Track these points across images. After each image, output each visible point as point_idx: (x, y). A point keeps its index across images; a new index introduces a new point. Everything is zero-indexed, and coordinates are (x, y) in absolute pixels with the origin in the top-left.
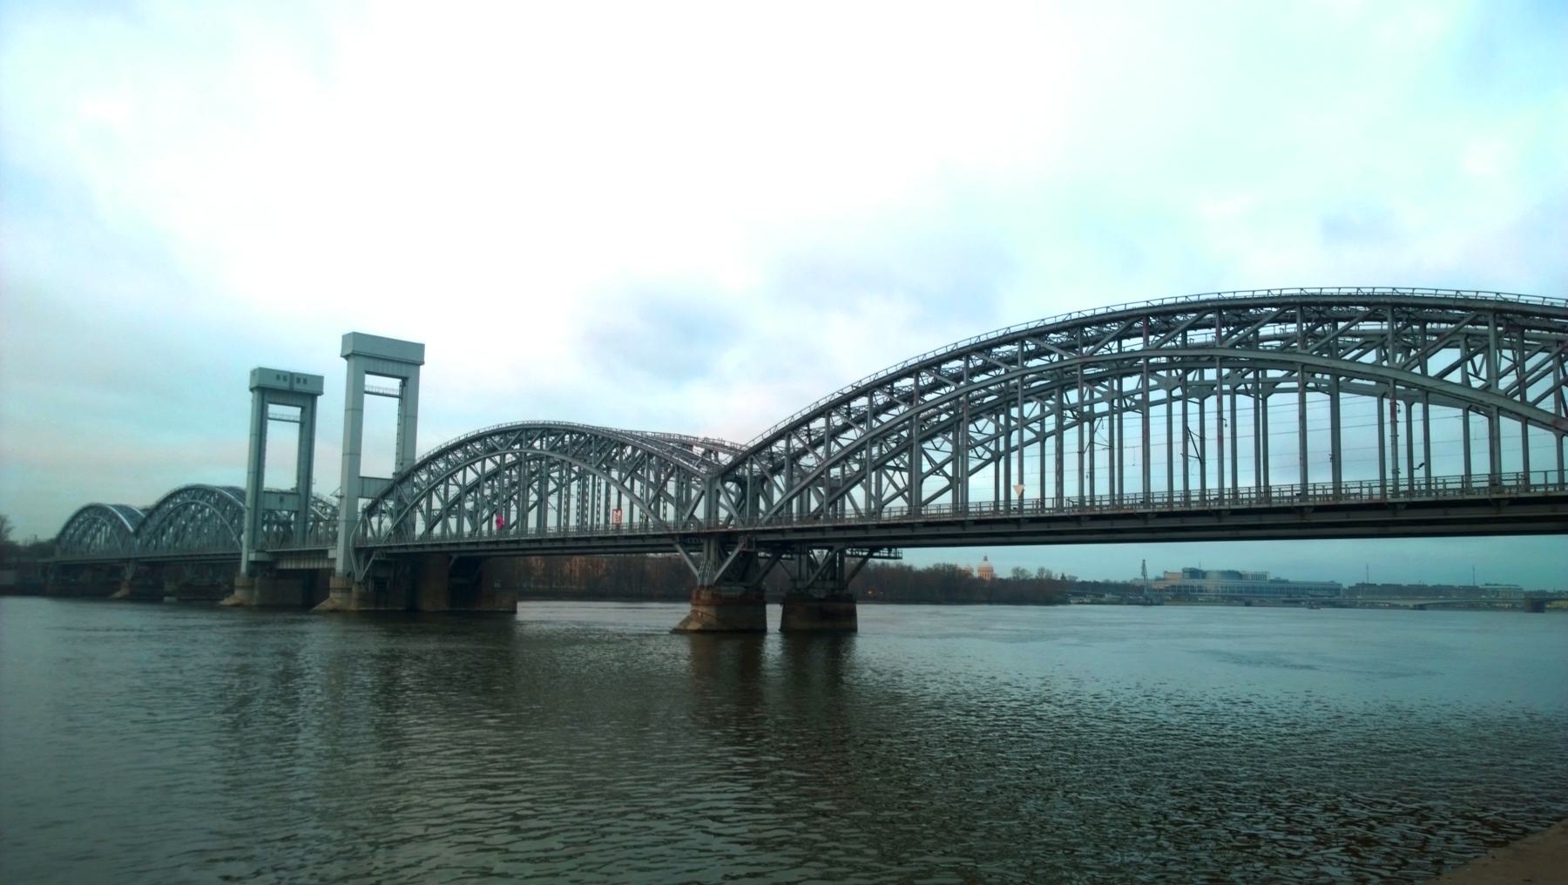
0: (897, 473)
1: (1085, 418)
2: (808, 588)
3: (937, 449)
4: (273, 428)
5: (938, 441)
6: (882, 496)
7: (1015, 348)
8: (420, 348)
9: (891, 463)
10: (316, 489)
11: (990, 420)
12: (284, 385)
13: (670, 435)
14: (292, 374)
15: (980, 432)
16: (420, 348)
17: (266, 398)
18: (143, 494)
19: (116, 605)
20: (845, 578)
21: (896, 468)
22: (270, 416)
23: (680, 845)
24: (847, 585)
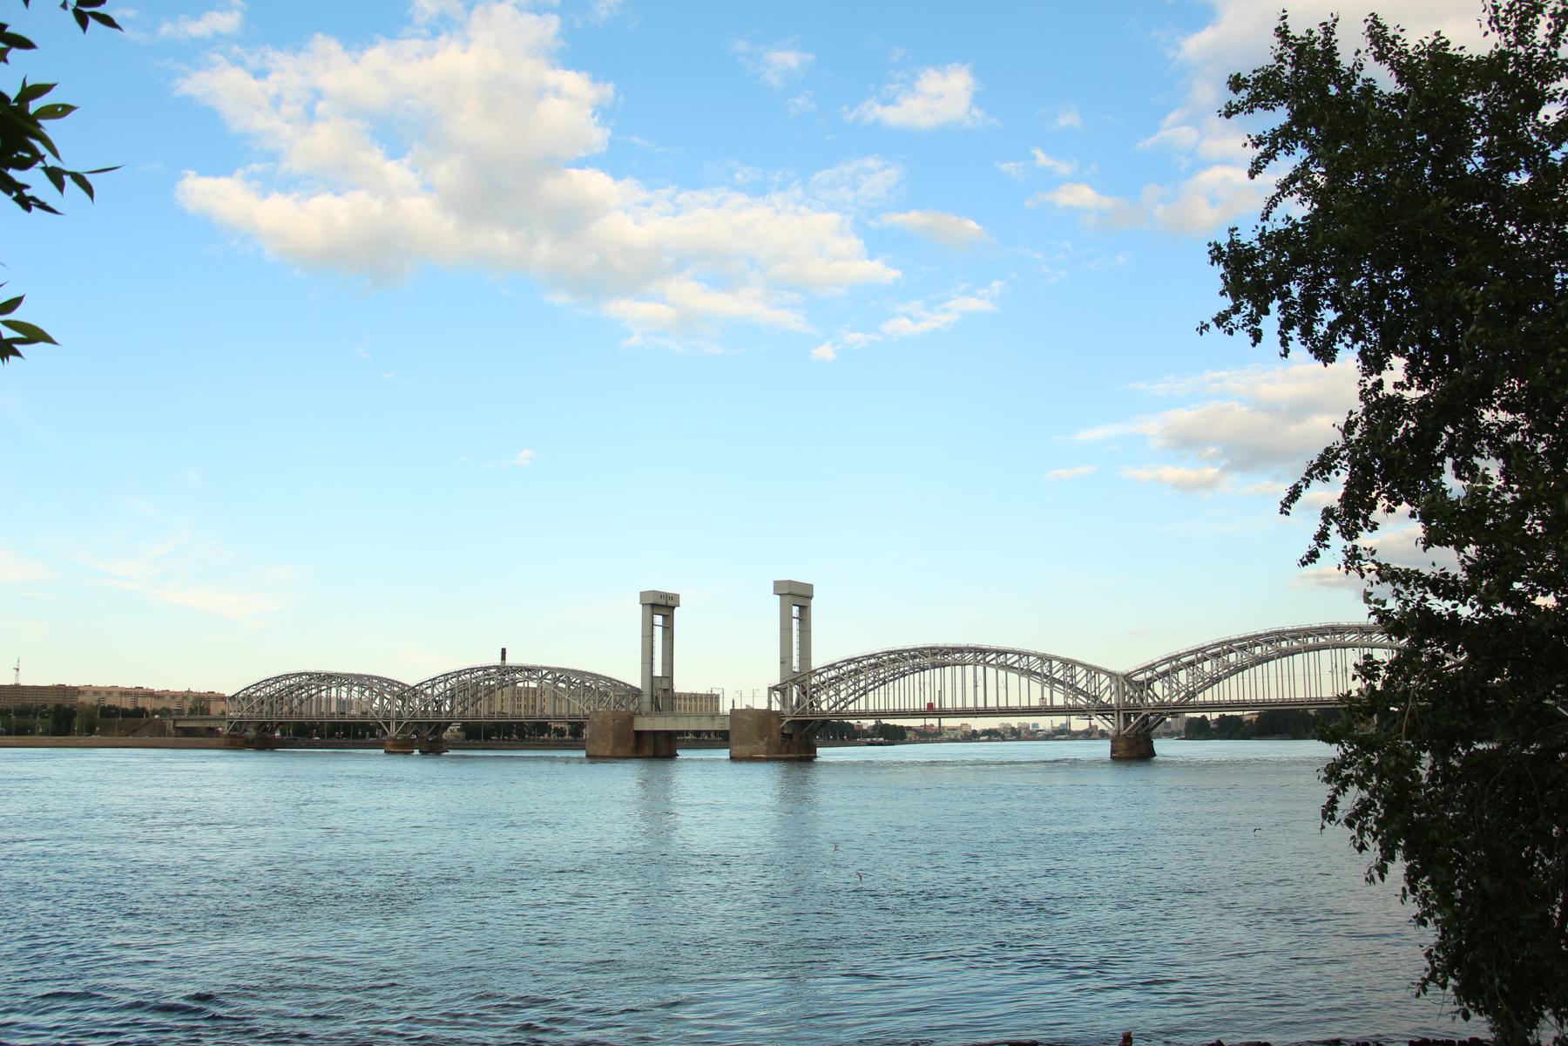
12: (663, 602)
14: (667, 594)
17: (655, 612)
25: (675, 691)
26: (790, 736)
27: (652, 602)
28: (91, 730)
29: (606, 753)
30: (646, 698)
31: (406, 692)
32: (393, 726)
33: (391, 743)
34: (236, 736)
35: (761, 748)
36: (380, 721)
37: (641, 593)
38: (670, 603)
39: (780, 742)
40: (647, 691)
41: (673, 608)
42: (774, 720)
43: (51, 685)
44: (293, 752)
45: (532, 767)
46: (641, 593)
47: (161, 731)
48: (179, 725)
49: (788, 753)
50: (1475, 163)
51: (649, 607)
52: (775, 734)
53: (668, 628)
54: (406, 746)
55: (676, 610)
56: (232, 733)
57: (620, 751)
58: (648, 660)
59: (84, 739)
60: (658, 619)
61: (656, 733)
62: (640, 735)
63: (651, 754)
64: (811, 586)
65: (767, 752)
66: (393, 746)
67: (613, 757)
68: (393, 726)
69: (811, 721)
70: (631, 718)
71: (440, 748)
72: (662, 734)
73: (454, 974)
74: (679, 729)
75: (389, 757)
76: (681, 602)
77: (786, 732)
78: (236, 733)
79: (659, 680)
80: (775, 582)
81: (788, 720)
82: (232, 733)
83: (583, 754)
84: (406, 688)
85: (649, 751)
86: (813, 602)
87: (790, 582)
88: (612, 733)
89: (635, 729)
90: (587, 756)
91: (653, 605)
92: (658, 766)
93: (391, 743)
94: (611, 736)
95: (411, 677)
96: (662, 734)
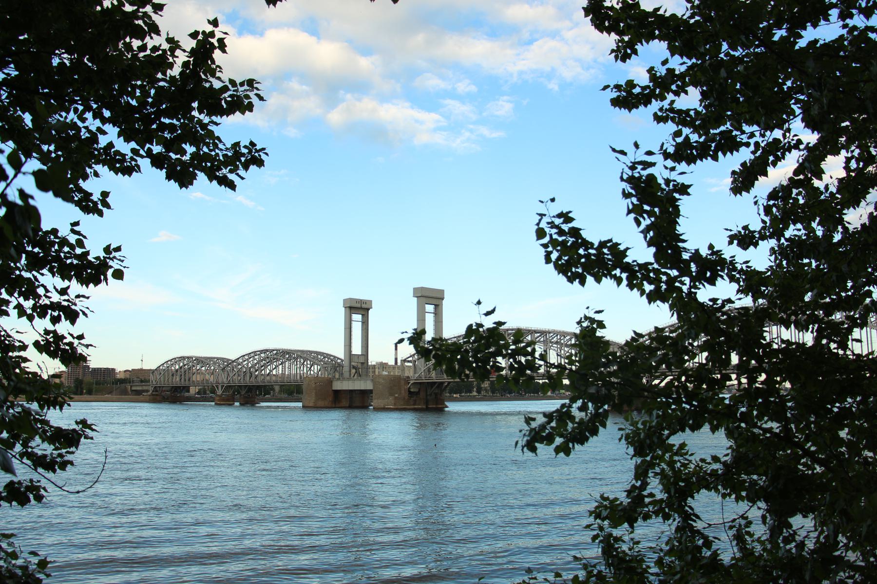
4: (354, 324)
8: (442, 291)
12: (358, 305)
16: (442, 291)
25: (370, 364)
26: (417, 393)
27: (349, 306)
28: (90, 392)
29: (311, 404)
30: (346, 369)
31: (226, 364)
32: (220, 388)
33: (218, 398)
34: (157, 395)
35: (390, 402)
36: (214, 385)
37: (443, 290)
38: (364, 306)
39: (407, 397)
40: (346, 364)
41: (368, 309)
42: (403, 382)
43: (640, 332)
44: (200, 404)
45: (325, 412)
46: (443, 290)
47: (124, 392)
48: (133, 388)
49: (414, 404)
50: (134, 103)
51: (348, 309)
52: (403, 392)
53: (365, 323)
54: (228, 400)
55: (370, 311)
56: (154, 393)
57: (321, 403)
58: (348, 344)
59: (86, 396)
60: (430, 308)
61: (351, 392)
62: (337, 393)
63: (348, 405)
64: (443, 291)
65: (395, 404)
66: (219, 400)
67: (316, 407)
68: (220, 388)
69: (436, 383)
70: (330, 382)
71: (254, 401)
72: (357, 392)
73: (347, 541)
74: (344, 389)
75: (242, 407)
76: (373, 305)
77: (412, 390)
78: (157, 393)
79: (357, 357)
80: (414, 289)
81: (412, 382)
82: (154, 393)
83: (300, 404)
84: (230, 362)
85: (345, 403)
86: (444, 302)
87: (422, 288)
88: (314, 391)
89: (333, 389)
90: (303, 407)
91: (351, 308)
92: (357, 414)
93: (218, 398)
94: (313, 393)
95: (232, 355)
96: (357, 392)
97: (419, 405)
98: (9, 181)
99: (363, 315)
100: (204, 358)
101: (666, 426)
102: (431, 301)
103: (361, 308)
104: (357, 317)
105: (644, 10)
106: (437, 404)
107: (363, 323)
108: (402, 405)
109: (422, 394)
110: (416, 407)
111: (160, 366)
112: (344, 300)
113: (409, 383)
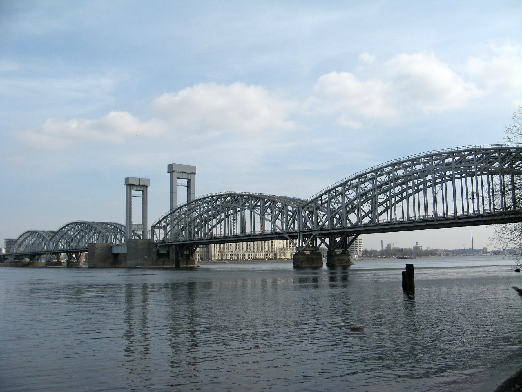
0: (336, 204)
1: (452, 179)
2: (303, 250)
3: (351, 194)
4: (134, 199)
5: (351, 191)
6: (173, 209)
7: (374, 174)
8: (194, 167)
9: (333, 200)
10: (362, 237)
11: (370, 183)
13: (245, 193)
15: (366, 187)
16: (194, 167)
17: (131, 189)
18: (375, 250)
19: (30, 268)
20: (318, 246)
21: (335, 202)
22: (132, 195)
23: (20, 300)
24: (318, 248)
26: (168, 254)
41: (146, 187)
55: (149, 188)
77: (161, 252)
81: (159, 245)
97: (168, 265)
98: (448, 252)
99: (143, 192)
100: (97, 223)
101: (391, 177)
102: (183, 176)
103: (139, 185)
104: (137, 194)
105: (380, 251)
106: (187, 264)
107: (143, 198)
108: (151, 265)
109: (173, 255)
110: (165, 266)
111: (62, 228)
112: (125, 179)
113: (157, 246)
